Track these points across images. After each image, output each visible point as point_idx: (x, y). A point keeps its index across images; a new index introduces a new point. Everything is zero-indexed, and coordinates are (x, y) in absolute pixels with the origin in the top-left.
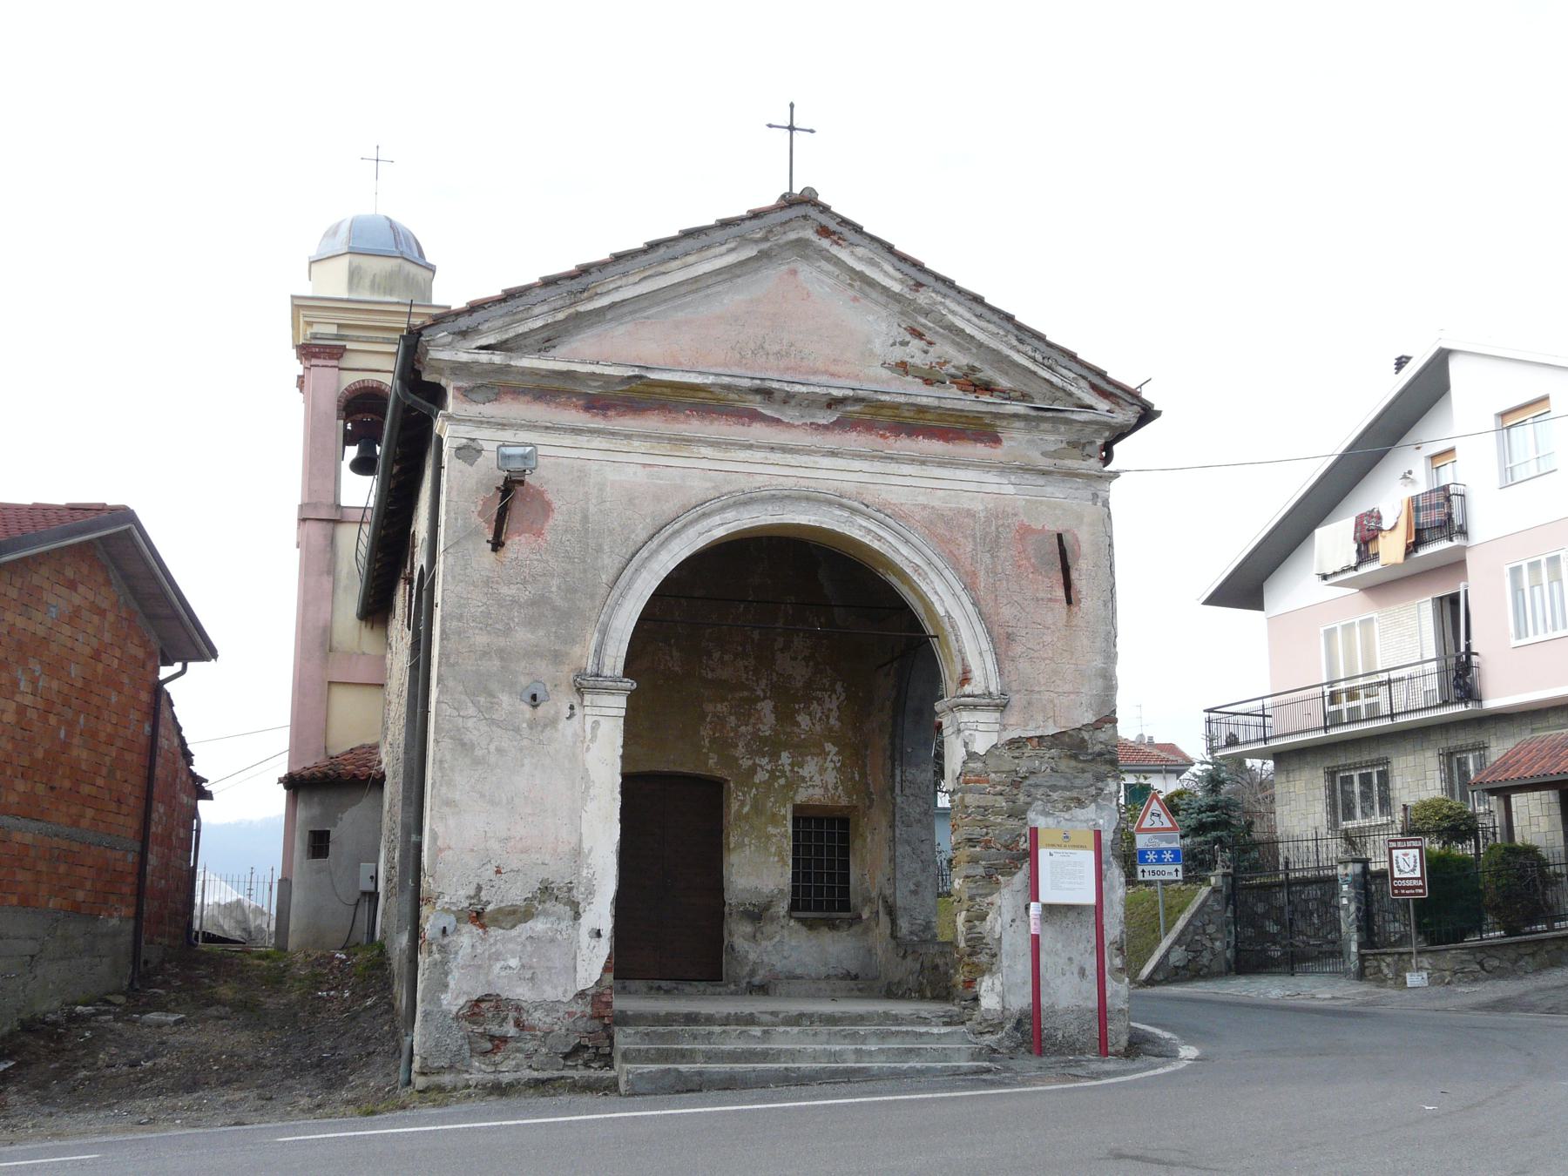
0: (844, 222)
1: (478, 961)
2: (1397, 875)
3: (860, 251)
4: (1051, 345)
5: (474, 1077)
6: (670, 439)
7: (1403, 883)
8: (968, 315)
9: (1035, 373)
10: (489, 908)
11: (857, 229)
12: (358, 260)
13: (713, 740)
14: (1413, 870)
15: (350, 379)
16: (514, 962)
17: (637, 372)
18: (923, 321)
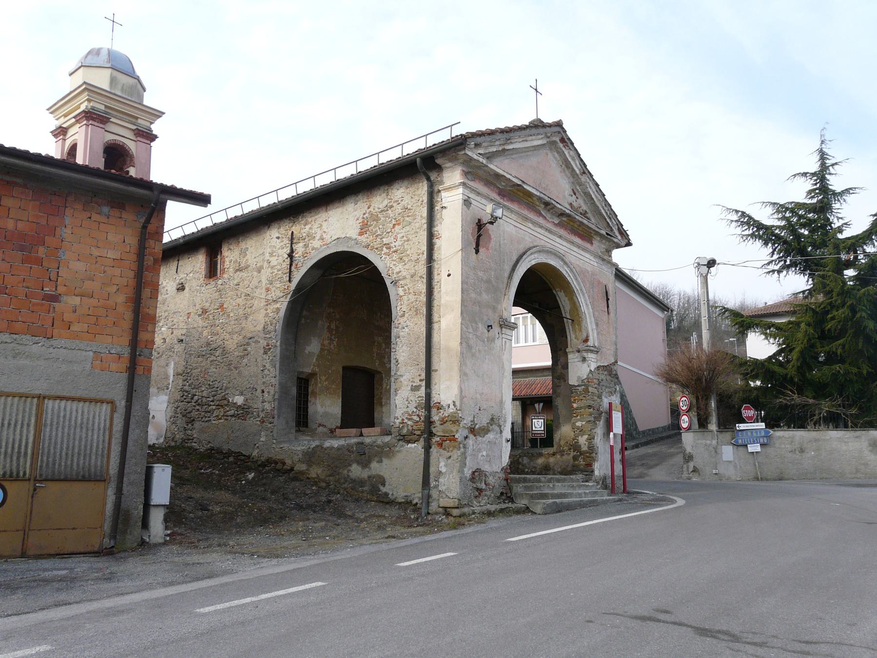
0: (569, 139)
1: (474, 453)
2: (534, 429)
3: (571, 153)
4: (612, 210)
5: (477, 509)
6: (523, 217)
7: (536, 432)
8: (594, 190)
9: (606, 219)
10: (477, 426)
11: (572, 144)
12: (115, 73)
13: (377, 354)
14: (541, 427)
15: (110, 137)
16: (484, 453)
17: (519, 183)
18: (578, 188)
